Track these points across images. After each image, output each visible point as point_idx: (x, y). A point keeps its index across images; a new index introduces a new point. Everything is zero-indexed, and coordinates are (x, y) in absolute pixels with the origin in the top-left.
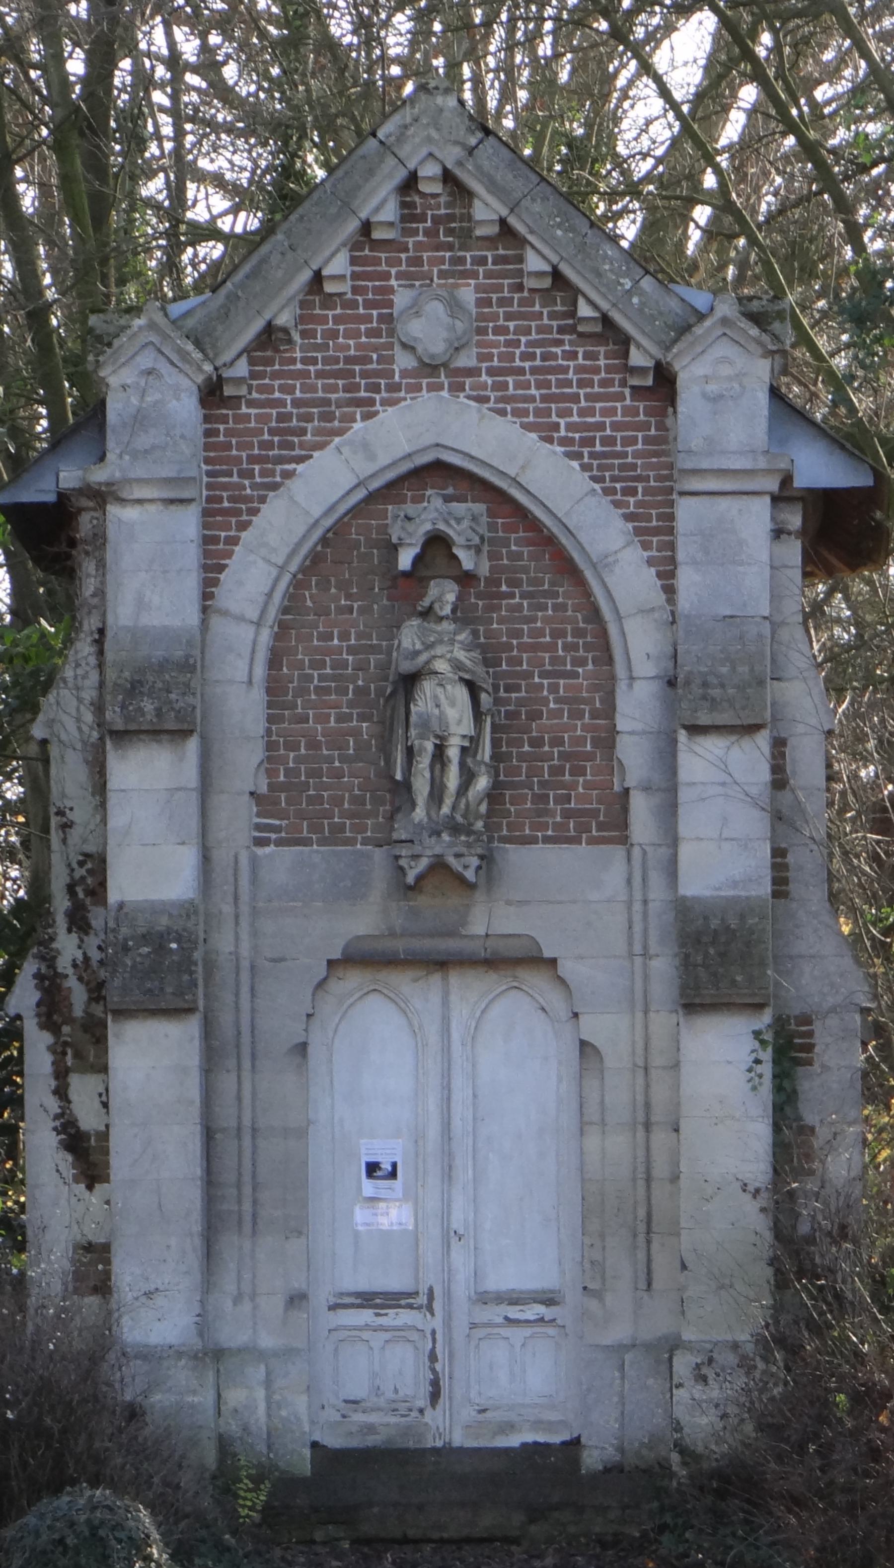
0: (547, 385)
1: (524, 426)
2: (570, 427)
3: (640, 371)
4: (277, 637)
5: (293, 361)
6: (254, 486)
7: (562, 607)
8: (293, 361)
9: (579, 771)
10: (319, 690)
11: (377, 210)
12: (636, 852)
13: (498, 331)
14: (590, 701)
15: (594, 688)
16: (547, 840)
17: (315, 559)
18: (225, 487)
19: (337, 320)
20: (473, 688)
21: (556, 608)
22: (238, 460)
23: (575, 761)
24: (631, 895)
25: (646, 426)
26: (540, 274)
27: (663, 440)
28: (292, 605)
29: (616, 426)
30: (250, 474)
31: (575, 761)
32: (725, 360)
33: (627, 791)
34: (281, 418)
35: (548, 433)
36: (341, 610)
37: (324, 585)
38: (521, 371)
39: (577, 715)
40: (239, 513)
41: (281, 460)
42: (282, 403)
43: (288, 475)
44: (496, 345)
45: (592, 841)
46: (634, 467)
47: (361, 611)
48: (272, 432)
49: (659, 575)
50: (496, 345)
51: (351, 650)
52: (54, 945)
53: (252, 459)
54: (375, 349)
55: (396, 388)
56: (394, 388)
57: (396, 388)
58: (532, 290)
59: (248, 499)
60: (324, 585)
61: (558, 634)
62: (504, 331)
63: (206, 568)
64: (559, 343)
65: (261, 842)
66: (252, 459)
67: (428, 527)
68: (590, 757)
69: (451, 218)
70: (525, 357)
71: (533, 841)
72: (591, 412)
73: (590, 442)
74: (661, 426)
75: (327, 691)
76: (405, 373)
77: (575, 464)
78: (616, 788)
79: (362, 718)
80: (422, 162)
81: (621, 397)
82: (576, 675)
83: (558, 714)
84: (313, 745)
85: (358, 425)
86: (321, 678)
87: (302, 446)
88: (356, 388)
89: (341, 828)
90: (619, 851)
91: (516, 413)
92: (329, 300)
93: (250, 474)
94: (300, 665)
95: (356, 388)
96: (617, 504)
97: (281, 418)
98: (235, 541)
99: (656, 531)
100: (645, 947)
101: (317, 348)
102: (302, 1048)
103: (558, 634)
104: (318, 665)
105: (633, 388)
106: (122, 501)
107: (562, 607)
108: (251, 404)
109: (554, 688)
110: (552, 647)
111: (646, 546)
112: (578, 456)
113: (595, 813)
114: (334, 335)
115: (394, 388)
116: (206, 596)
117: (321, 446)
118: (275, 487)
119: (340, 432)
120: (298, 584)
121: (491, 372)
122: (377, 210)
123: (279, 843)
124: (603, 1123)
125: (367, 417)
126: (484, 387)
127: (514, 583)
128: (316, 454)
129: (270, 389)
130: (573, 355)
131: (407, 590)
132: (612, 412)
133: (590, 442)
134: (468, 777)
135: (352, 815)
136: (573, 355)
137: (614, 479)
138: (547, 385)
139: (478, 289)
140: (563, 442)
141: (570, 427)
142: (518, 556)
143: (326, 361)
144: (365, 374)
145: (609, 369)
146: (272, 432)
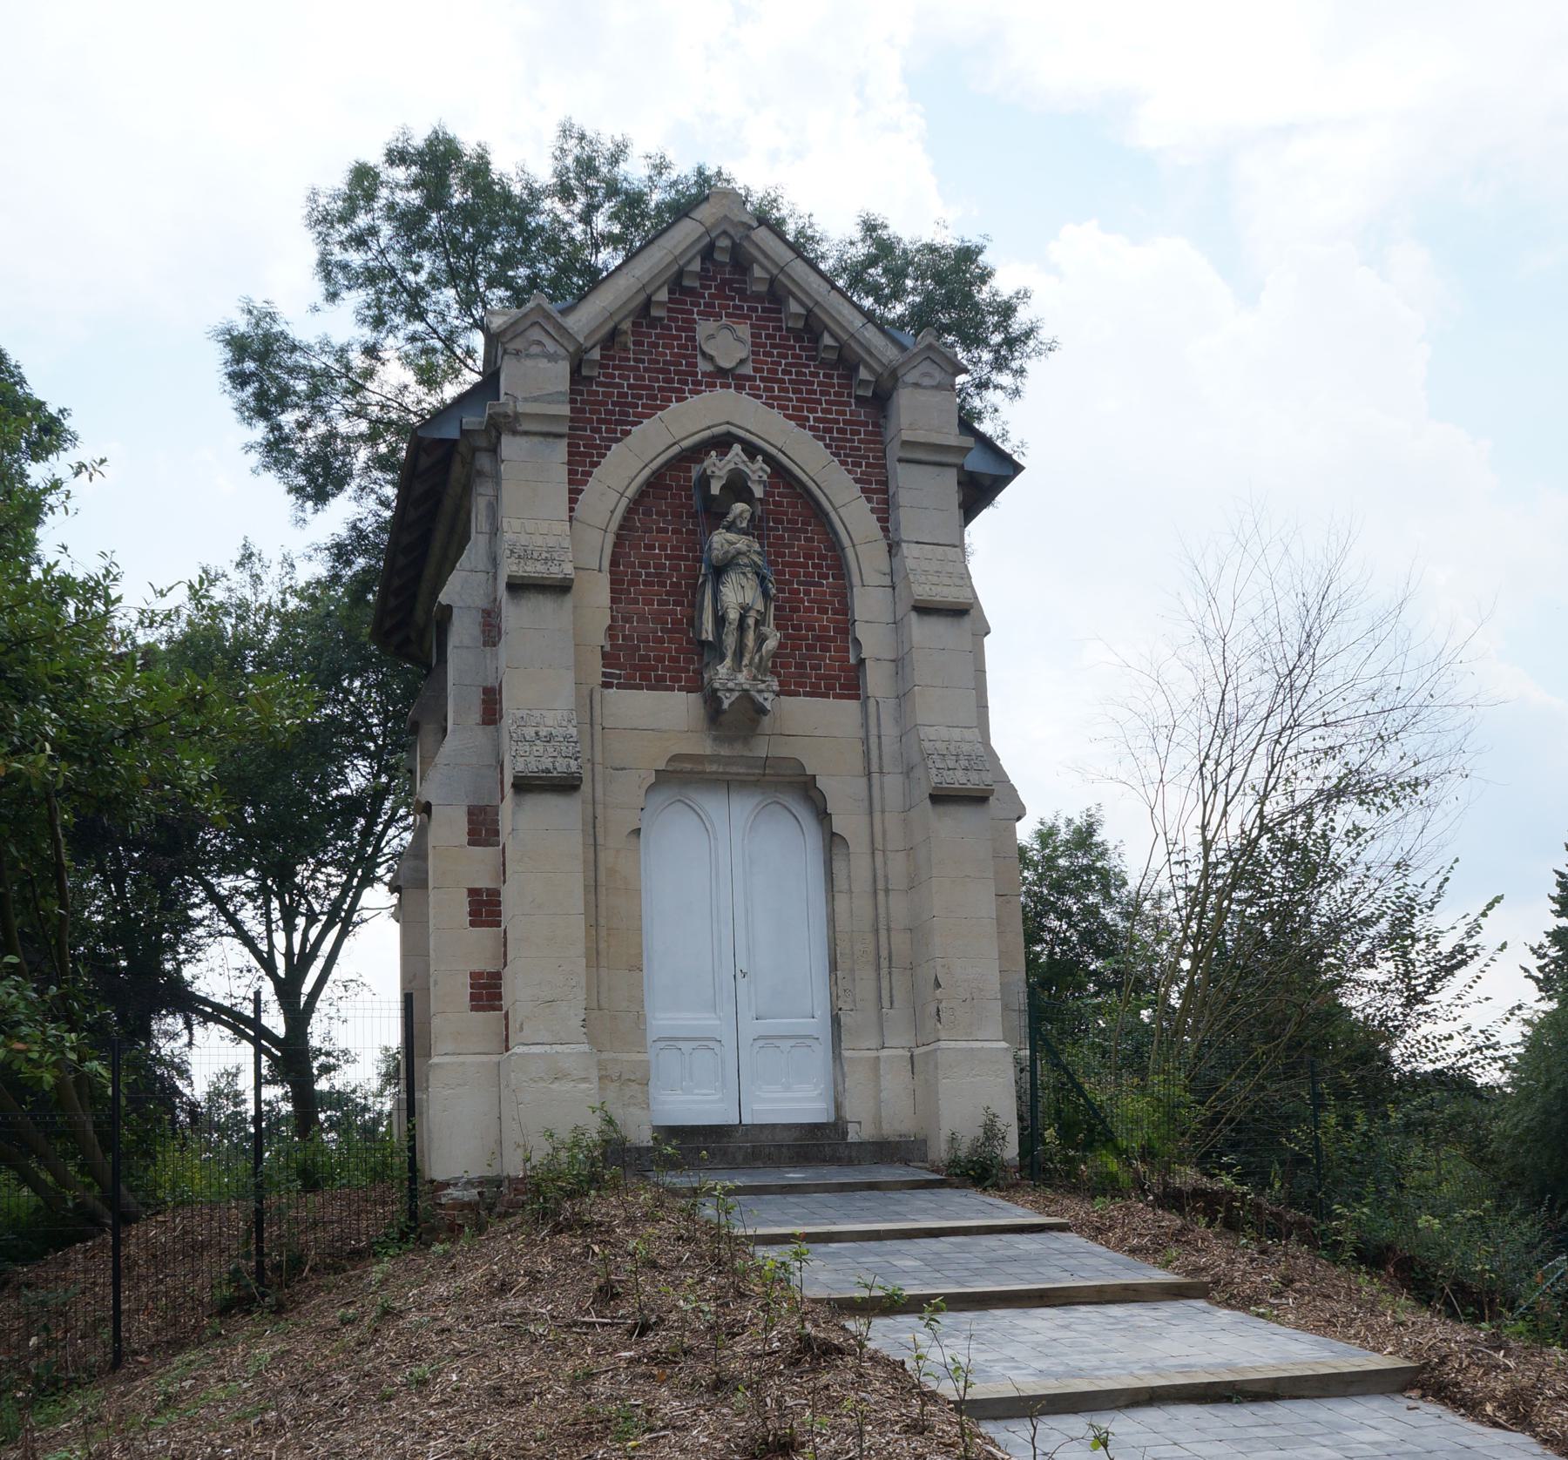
0: (801, 392)
1: (786, 416)
2: (816, 419)
3: (864, 383)
4: (616, 545)
5: (628, 360)
6: (602, 439)
7: (811, 540)
8: (628, 360)
9: (825, 649)
10: (645, 583)
11: (689, 262)
12: (872, 702)
13: (766, 354)
14: (832, 603)
15: (833, 595)
16: (806, 694)
17: (642, 494)
18: (581, 437)
19: (658, 336)
20: (762, 580)
21: (806, 539)
22: (590, 421)
23: (823, 640)
24: (867, 732)
25: (866, 424)
26: (798, 316)
27: (880, 434)
28: (626, 524)
29: (846, 422)
30: (599, 431)
31: (823, 640)
32: (925, 375)
33: (862, 662)
34: (620, 395)
35: (801, 422)
36: (660, 530)
37: (647, 513)
38: (782, 381)
39: (823, 611)
40: (592, 455)
41: (618, 423)
42: (620, 386)
43: (628, 433)
44: (766, 363)
45: (836, 696)
46: (859, 449)
47: (675, 532)
48: (614, 404)
49: (879, 520)
50: (766, 363)
51: (667, 557)
52: (1097, 839)
53: (600, 421)
54: (684, 356)
55: (699, 383)
56: (697, 383)
57: (699, 383)
58: (788, 329)
59: (599, 447)
60: (647, 513)
61: (808, 557)
62: (770, 354)
63: (571, 491)
64: (808, 366)
65: (606, 685)
66: (600, 421)
67: (732, 466)
68: (833, 639)
69: (732, 281)
70: (785, 372)
71: (797, 694)
72: (829, 411)
73: (830, 431)
74: (876, 425)
75: (651, 584)
76: (704, 374)
77: (821, 444)
78: (852, 661)
79: (676, 603)
80: (718, 236)
81: (848, 404)
82: (822, 585)
83: (810, 610)
84: (642, 619)
85: (673, 405)
86: (647, 575)
87: (635, 415)
88: (671, 381)
89: (663, 678)
90: (853, 705)
91: (780, 407)
92: (652, 325)
93: (599, 431)
94: (632, 565)
95: (671, 381)
96: (849, 472)
97: (620, 395)
98: (590, 474)
99: (875, 491)
100: (881, 768)
101: (644, 353)
102: (637, 832)
103: (808, 557)
104: (645, 566)
105: (857, 397)
106: (515, 433)
107: (811, 540)
108: (599, 384)
109: (807, 593)
110: (805, 566)
111: (869, 500)
112: (822, 439)
113: (838, 678)
114: (656, 345)
115: (697, 383)
116: (571, 510)
117: (649, 416)
118: (617, 440)
119: (662, 408)
120: (630, 511)
121: (762, 379)
122: (689, 262)
123: (619, 686)
124: (850, 891)
125: (679, 400)
126: (758, 388)
127: (778, 521)
128: (614, 446)
129: (613, 376)
130: (816, 375)
131: (714, 513)
132: (844, 413)
133: (830, 431)
134: (761, 639)
135: (669, 669)
136: (816, 375)
137: (846, 455)
138: (801, 392)
139: (752, 326)
140: (812, 428)
141: (816, 419)
142: (779, 504)
143: (650, 361)
144: (677, 372)
145: (840, 386)
146: (614, 404)
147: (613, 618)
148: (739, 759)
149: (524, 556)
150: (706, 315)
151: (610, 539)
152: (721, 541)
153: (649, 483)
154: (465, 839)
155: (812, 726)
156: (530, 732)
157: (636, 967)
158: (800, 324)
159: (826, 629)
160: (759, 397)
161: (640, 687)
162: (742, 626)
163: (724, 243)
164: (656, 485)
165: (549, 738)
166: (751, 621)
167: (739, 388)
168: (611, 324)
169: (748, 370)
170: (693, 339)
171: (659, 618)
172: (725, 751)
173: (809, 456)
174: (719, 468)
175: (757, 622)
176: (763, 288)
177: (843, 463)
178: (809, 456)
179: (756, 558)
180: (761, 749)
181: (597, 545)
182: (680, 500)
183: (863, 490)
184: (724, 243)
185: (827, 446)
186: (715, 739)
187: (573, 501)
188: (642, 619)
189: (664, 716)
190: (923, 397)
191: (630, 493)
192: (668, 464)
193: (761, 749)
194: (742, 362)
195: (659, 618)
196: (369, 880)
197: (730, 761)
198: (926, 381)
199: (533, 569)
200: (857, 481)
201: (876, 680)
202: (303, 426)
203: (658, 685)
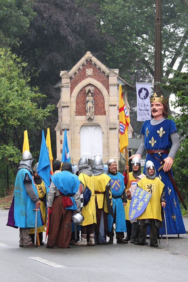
2: (101, 80)
13: (95, 72)
17: (80, 92)
29: (105, 80)
35: (99, 81)
37: (81, 94)
43: (77, 85)
45: (103, 115)
57: (86, 77)
60: (81, 94)
61: (100, 98)
76: (87, 76)
92: (81, 70)
102: (79, 133)
104: (80, 101)
125: (84, 80)
127: (96, 93)
147: (76, 107)
148: (90, 123)
149: (64, 103)
150: (87, 68)
151: (76, 98)
152: (88, 98)
153: (81, 90)
154: (60, 134)
155: (99, 119)
156: (64, 124)
157: (103, 144)
158: (98, 68)
159: (102, 107)
160: (93, 78)
161: (79, 115)
162: (90, 108)
163: (88, 59)
164: (81, 90)
165: (66, 124)
166: (91, 108)
167: (91, 77)
168: (74, 72)
169: (92, 75)
170: (85, 72)
171: (82, 107)
172: (89, 123)
173: (99, 85)
174: (87, 89)
175: (92, 108)
176: (94, 64)
177: (104, 86)
178: (99, 85)
179: (92, 100)
180: (94, 122)
181: (74, 99)
182: (83, 93)
183: (106, 89)
184: (88, 59)
185: (102, 84)
186: (88, 121)
187: (71, 94)
188: (80, 107)
189: (82, 119)
190: (112, 78)
191: (78, 92)
192: (83, 88)
193: (94, 122)
194: (91, 74)
195: (82, 107)
196: (181, 106)
197: (90, 124)
198: (113, 76)
199: (65, 105)
200: (106, 88)
201: (107, 113)
202: (97, 26)
203: (82, 115)
